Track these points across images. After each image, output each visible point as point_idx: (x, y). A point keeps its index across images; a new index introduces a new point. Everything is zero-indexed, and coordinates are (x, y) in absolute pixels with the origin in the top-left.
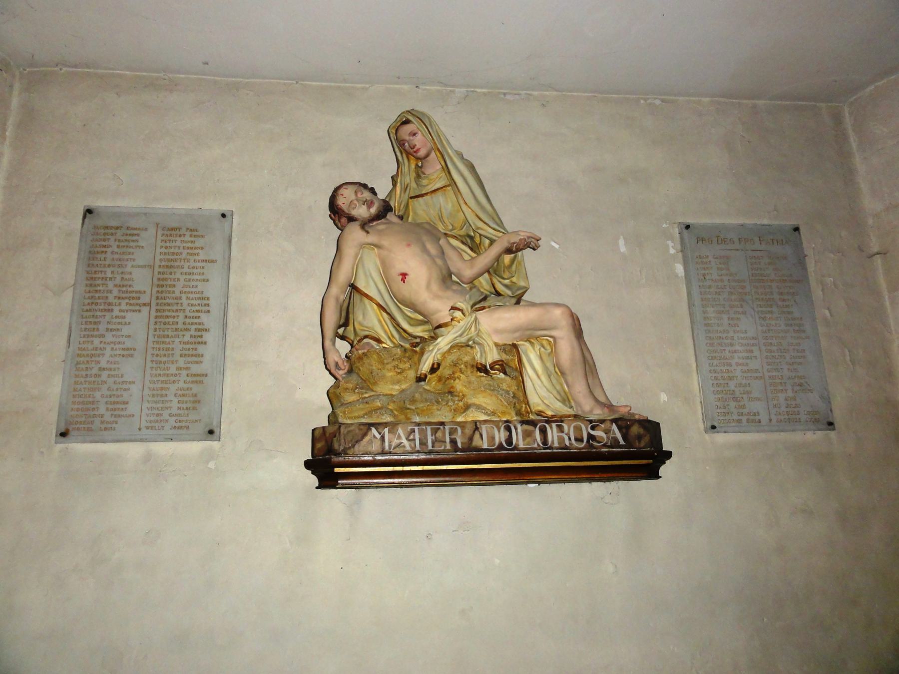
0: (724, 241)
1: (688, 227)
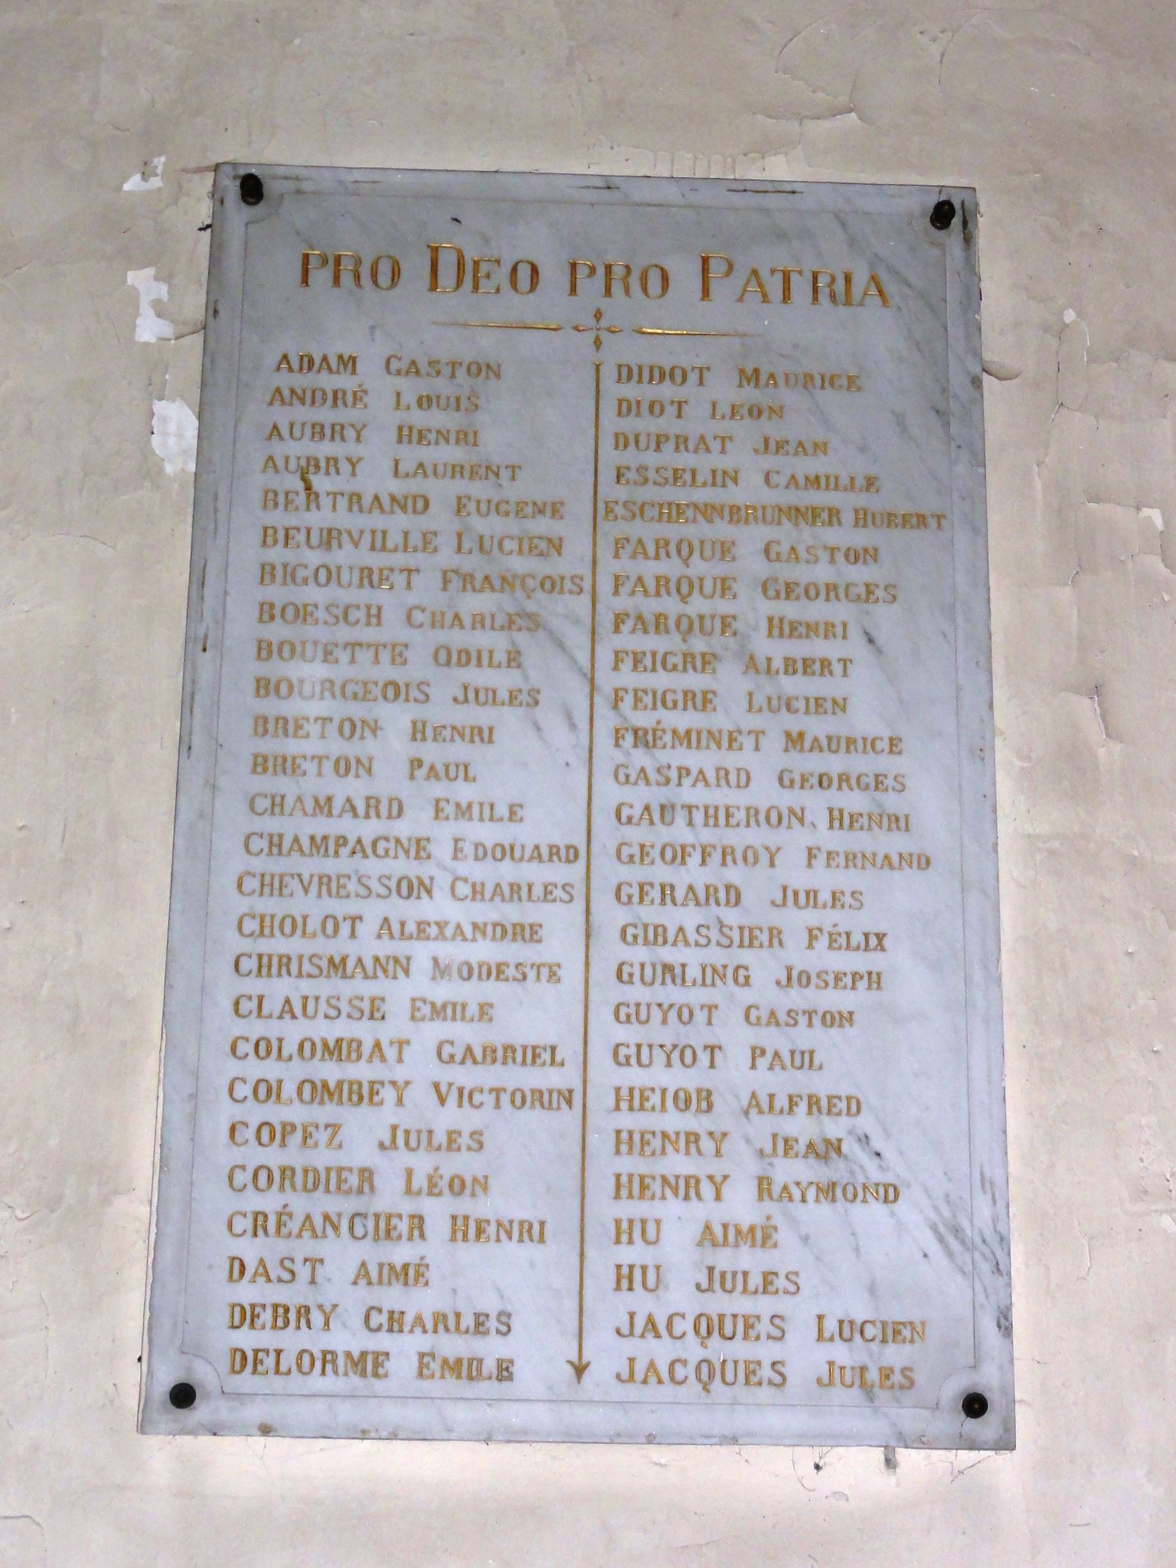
0: (469, 274)
1: (252, 189)
